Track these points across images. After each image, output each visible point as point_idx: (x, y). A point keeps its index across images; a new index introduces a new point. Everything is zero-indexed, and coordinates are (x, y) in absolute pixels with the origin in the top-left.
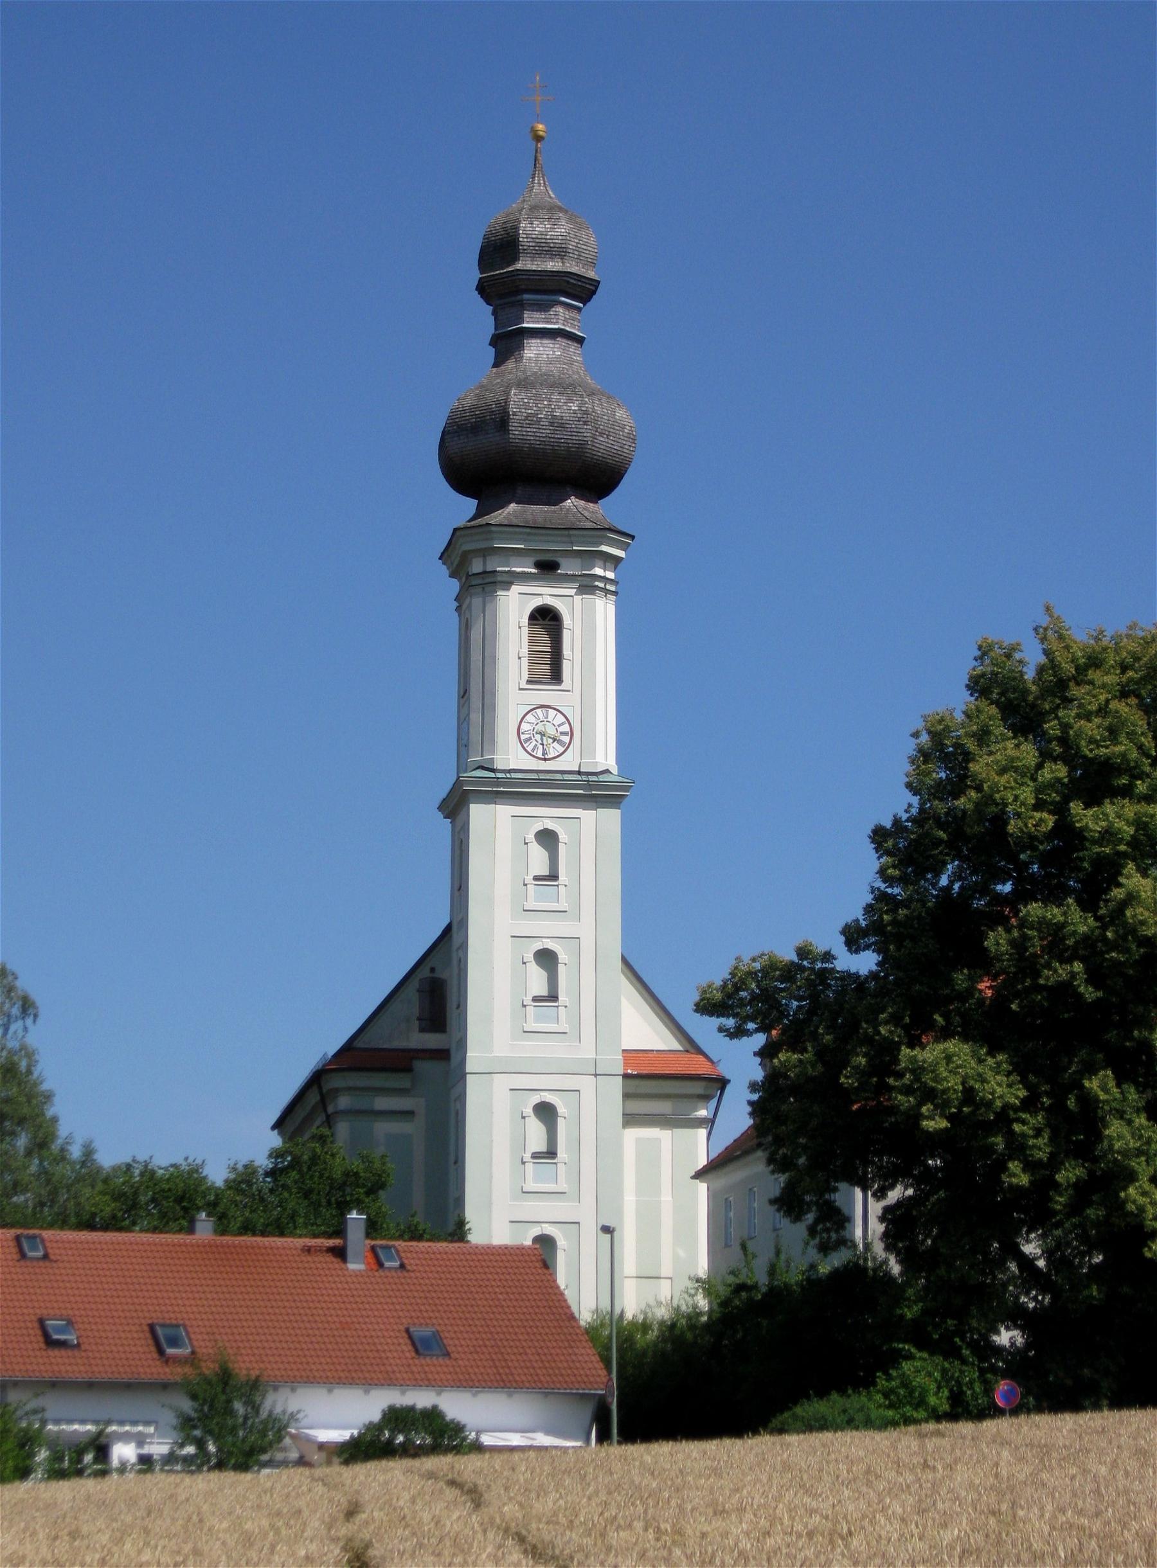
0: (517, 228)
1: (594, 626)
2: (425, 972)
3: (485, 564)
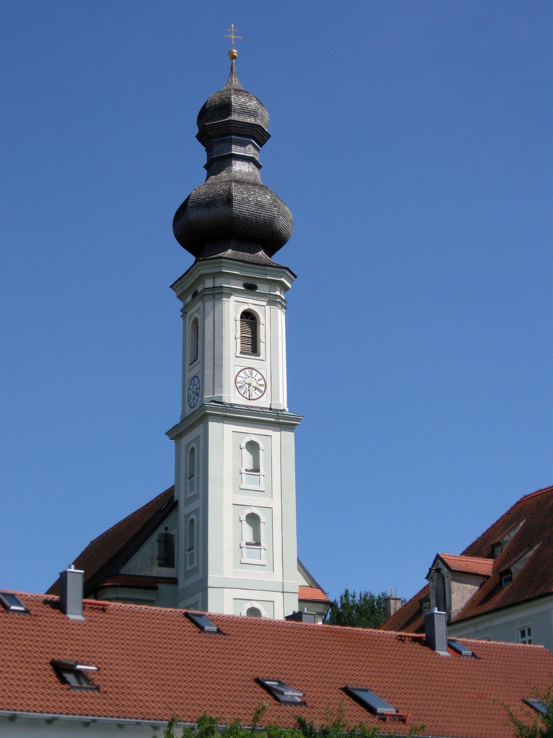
0: (229, 99)
1: (274, 323)
3: (214, 282)
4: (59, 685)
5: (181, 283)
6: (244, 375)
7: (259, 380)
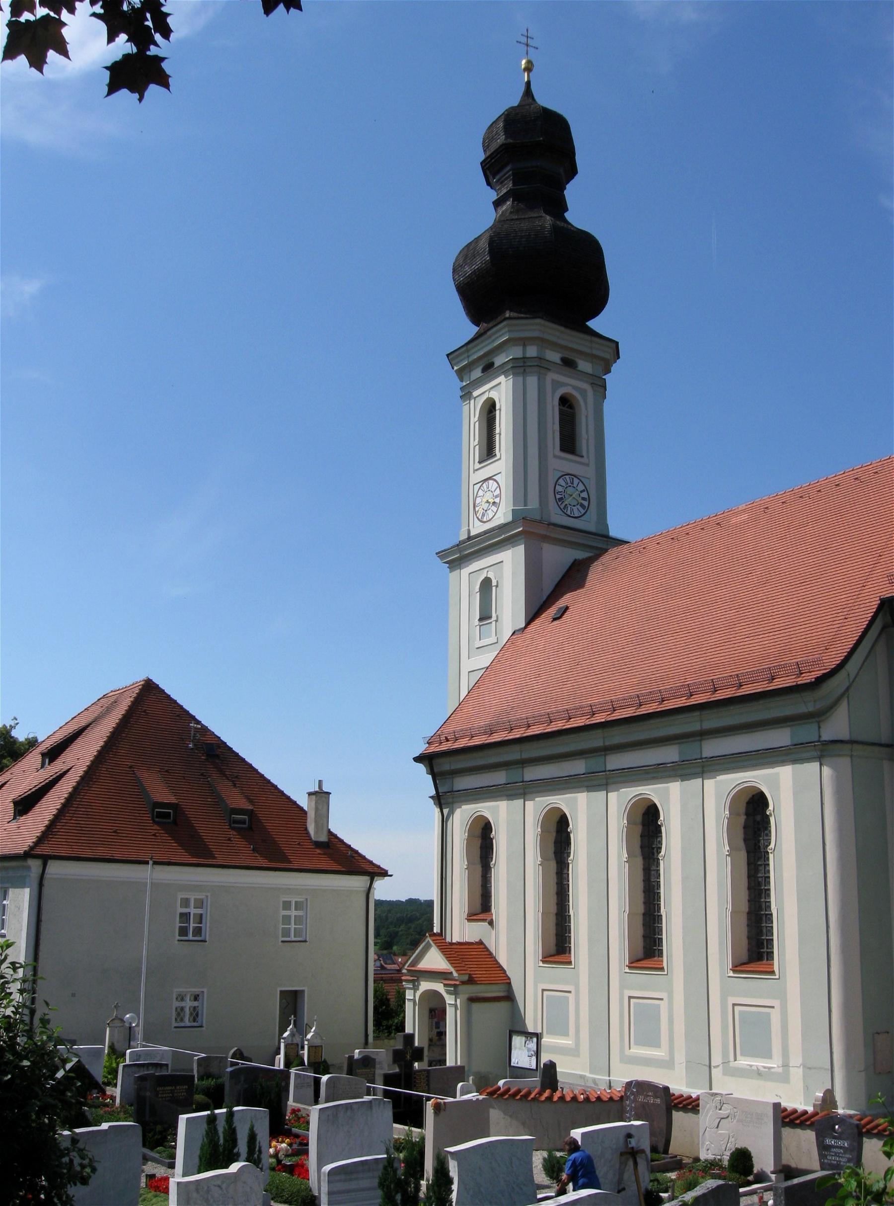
3: (524, 351)
5: (468, 351)
6: (563, 483)
7: (581, 492)
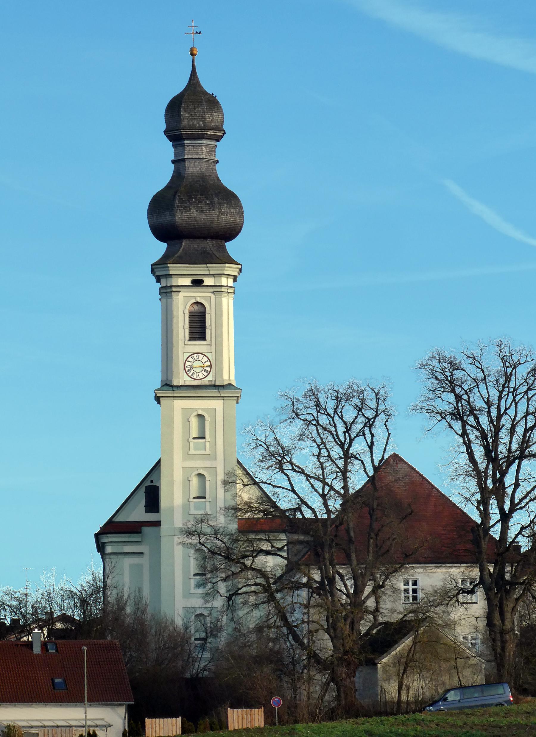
2: (148, 483)
4: (375, 444)
